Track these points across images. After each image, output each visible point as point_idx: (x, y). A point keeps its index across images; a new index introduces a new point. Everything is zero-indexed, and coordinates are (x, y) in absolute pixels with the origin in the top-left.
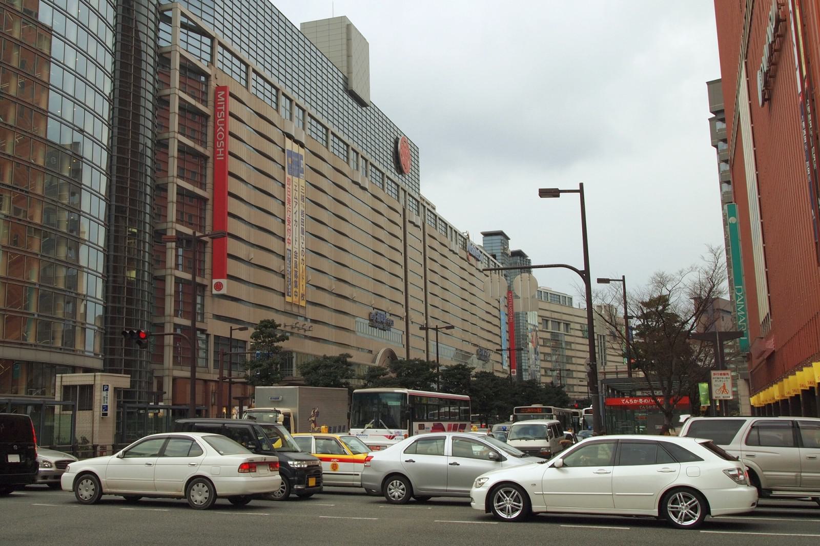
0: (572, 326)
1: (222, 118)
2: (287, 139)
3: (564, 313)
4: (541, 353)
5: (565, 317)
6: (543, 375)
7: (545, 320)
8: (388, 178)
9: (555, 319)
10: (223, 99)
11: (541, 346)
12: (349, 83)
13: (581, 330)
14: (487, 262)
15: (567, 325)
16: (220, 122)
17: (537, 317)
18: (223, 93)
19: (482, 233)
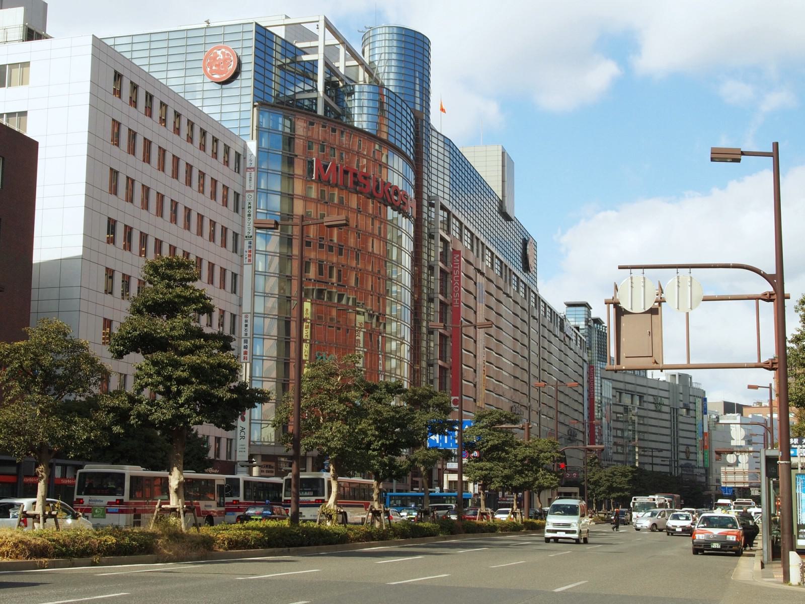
0: (645, 398)
1: (457, 275)
2: (478, 275)
3: (638, 385)
4: (614, 428)
5: (639, 389)
6: (614, 453)
7: (620, 392)
8: (466, 228)
9: (628, 391)
10: (458, 261)
11: (614, 420)
12: (503, 207)
13: (653, 403)
14: (457, 230)
15: (641, 397)
16: (456, 278)
17: (611, 389)
18: (458, 255)
19: (565, 304)
